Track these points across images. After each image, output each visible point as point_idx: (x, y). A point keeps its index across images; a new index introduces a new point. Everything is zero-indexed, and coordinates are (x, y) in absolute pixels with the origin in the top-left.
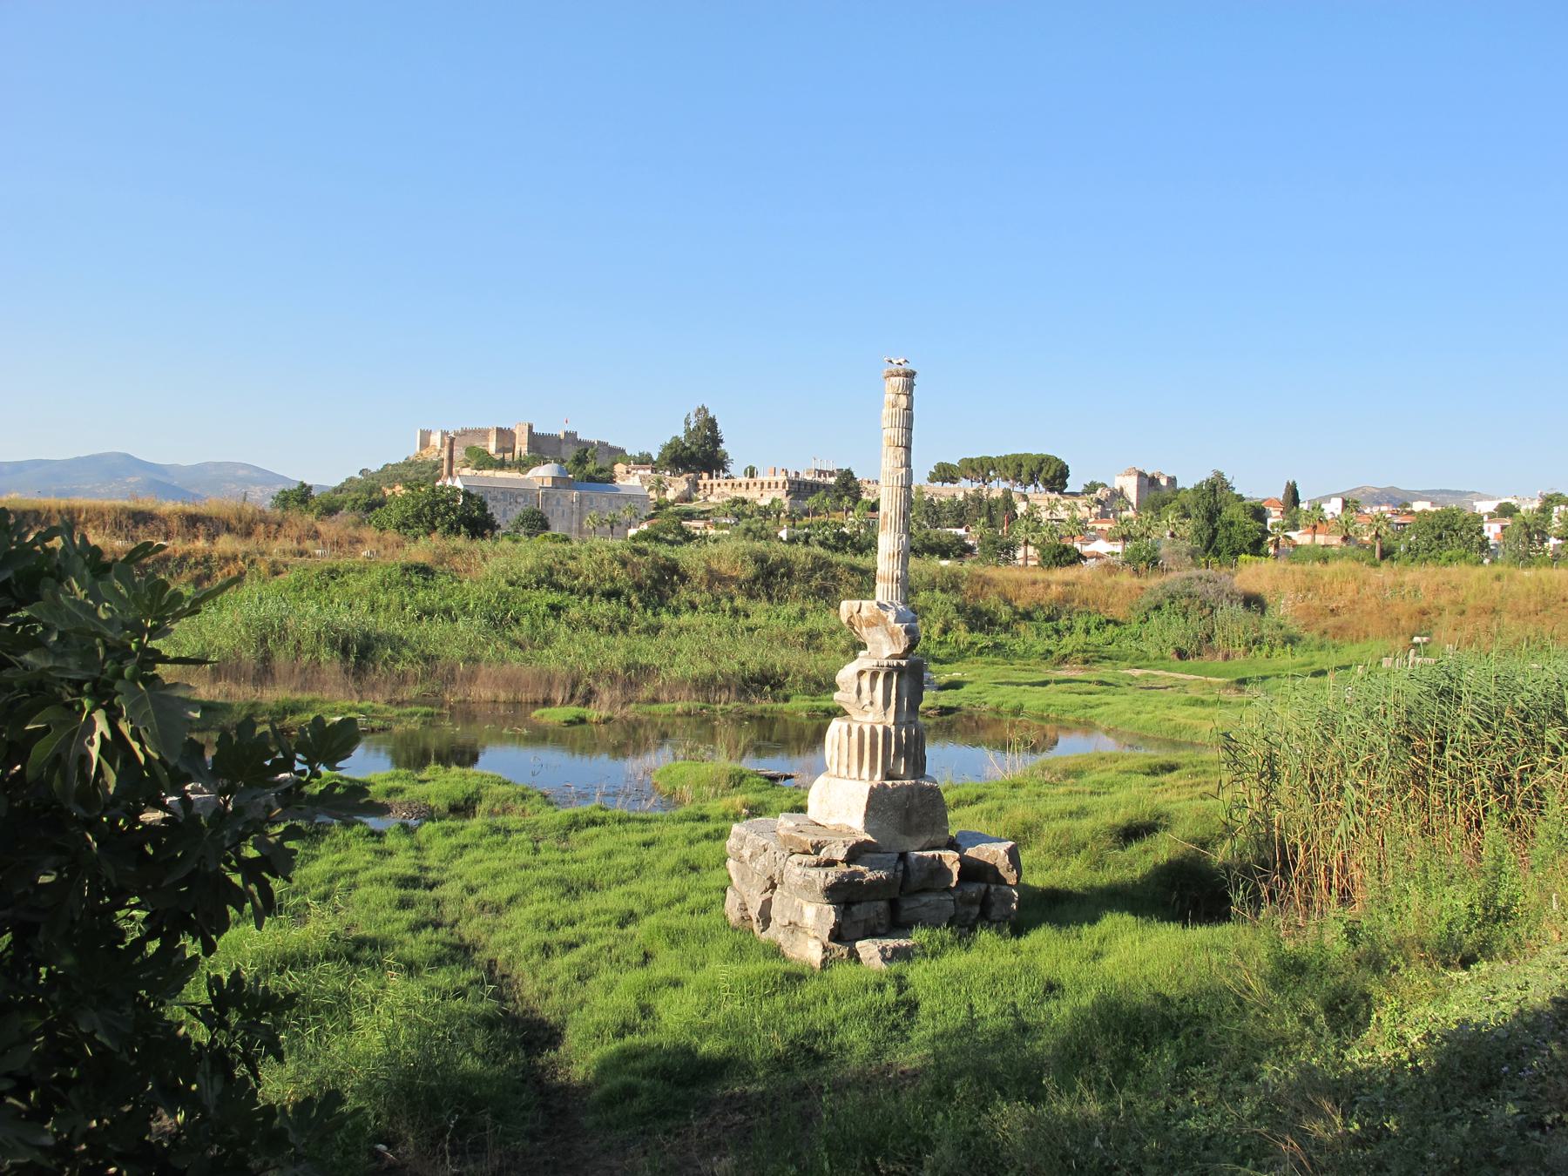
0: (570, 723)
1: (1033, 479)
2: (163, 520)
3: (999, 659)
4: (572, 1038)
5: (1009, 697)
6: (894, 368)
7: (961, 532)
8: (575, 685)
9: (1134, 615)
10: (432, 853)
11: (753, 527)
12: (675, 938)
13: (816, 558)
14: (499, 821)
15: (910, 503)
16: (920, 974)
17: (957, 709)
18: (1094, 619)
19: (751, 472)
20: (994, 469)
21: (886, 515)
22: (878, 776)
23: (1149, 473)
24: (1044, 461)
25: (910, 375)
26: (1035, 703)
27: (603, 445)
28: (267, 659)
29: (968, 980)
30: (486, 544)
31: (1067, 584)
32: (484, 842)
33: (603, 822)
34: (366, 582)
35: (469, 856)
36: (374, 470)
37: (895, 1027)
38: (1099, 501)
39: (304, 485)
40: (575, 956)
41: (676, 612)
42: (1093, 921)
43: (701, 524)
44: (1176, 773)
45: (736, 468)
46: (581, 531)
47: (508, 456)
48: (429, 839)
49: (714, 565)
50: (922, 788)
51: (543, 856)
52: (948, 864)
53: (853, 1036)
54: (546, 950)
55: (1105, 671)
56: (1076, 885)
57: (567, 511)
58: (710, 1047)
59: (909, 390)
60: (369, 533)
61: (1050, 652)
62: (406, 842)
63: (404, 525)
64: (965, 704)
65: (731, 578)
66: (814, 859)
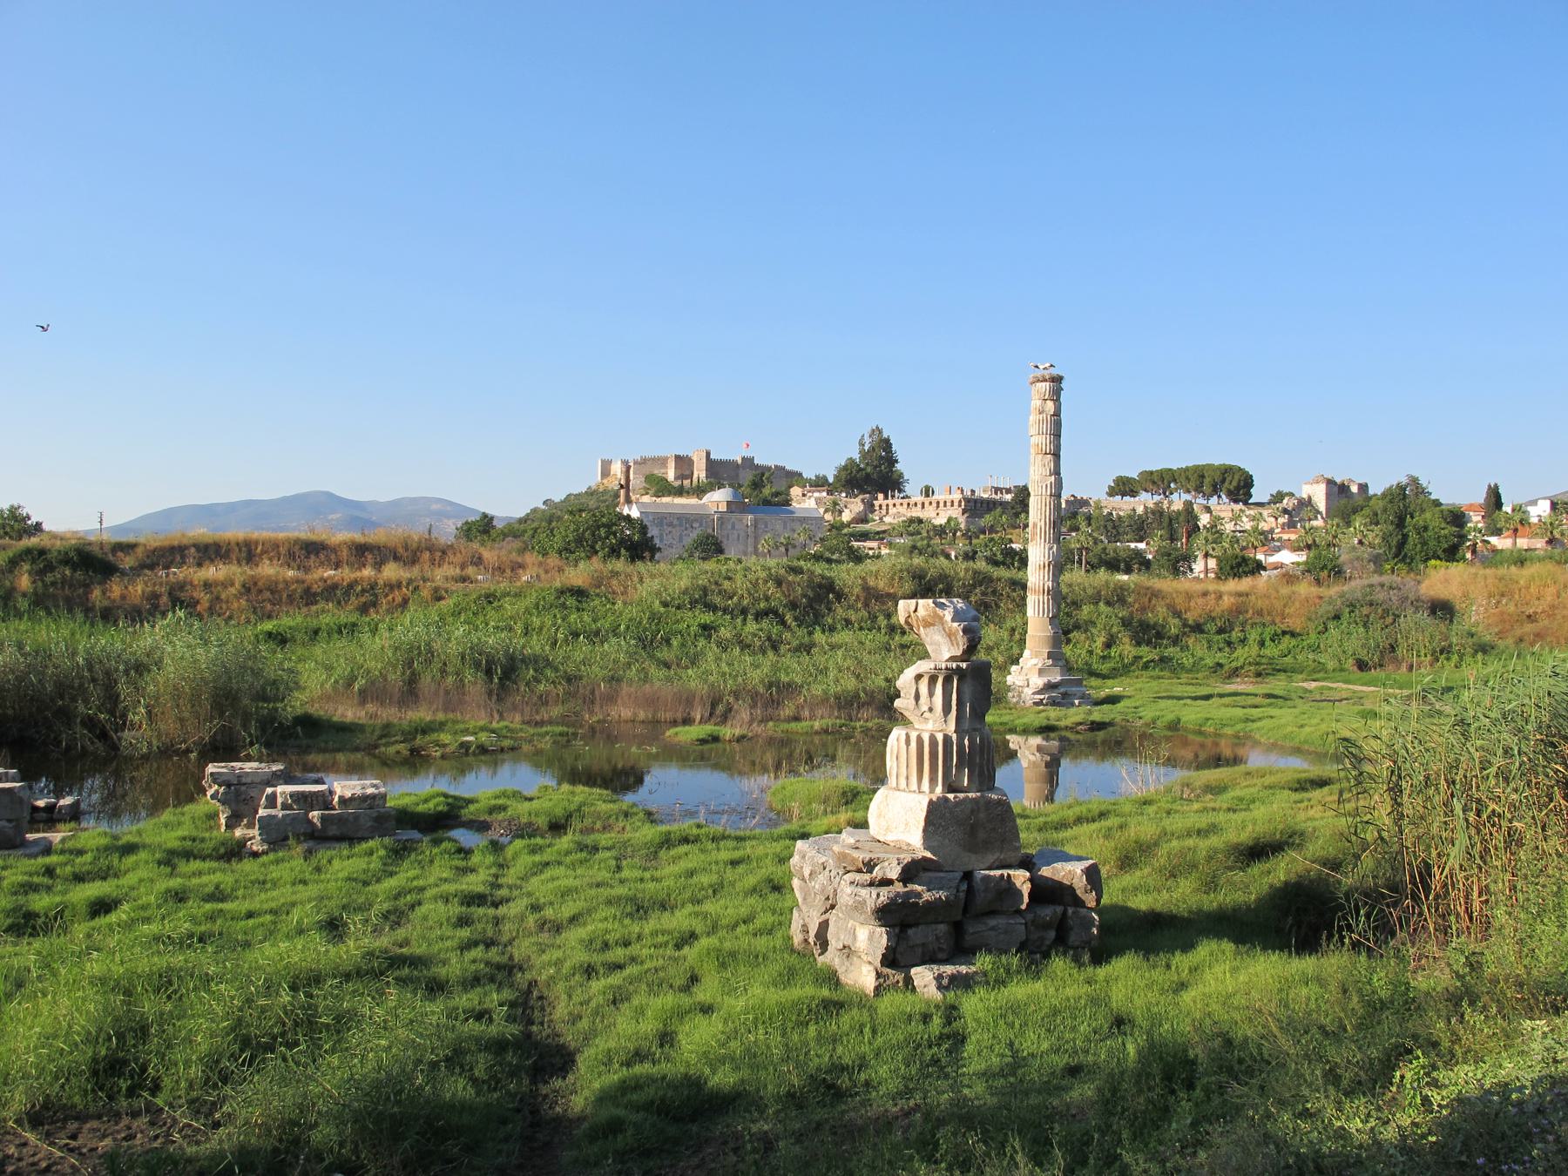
0: (703, 741)
1: (1215, 490)
2: (334, 550)
3: (1166, 673)
4: (583, 1062)
5: (1168, 711)
6: (1039, 373)
7: (1142, 546)
8: (713, 706)
9: (1311, 625)
10: (512, 871)
12: (725, 960)
14: (589, 840)
15: (1068, 516)
16: (973, 1004)
17: (1111, 724)
18: (1269, 631)
19: (928, 491)
20: (1175, 481)
22: (939, 789)
23: (1338, 481)
24: (1227, 471)
25: (1057, 380)
26: (1193, 717)
27: (780, 469)
28: (412, 682)
29: (1026, 1011)
31: (1240, 594)
32: (568, 859)
33: (696, 840)
34: (521, 605)
35: (548, 874)
36: (557, 500)
37: (935, 1061)
38: (1285, 511)
39: (485, 516)
40: (616, 979)
41: (832, 629)
42: (1187, 947)
43: (874, 544)
44: (1326, 789)
45: (913, 489)
46: (756, 552)
47: (687, 482)
48: (516, 855)
49: (871, 583)
50: (990, 801)
51: (626, 874)
52: (1018, 884)
53: (883, 1071)
54: (589, 971)
55: (1277, 685)
56: (1182, 910)
57: (742, 534)
58: (723, 1079)
59: (1056, 395)
60: (530, 558)
61: (1220, 665)
62: (490, 859)
63: (565, 550)
64: (1119, 719)
66: (867, 877)
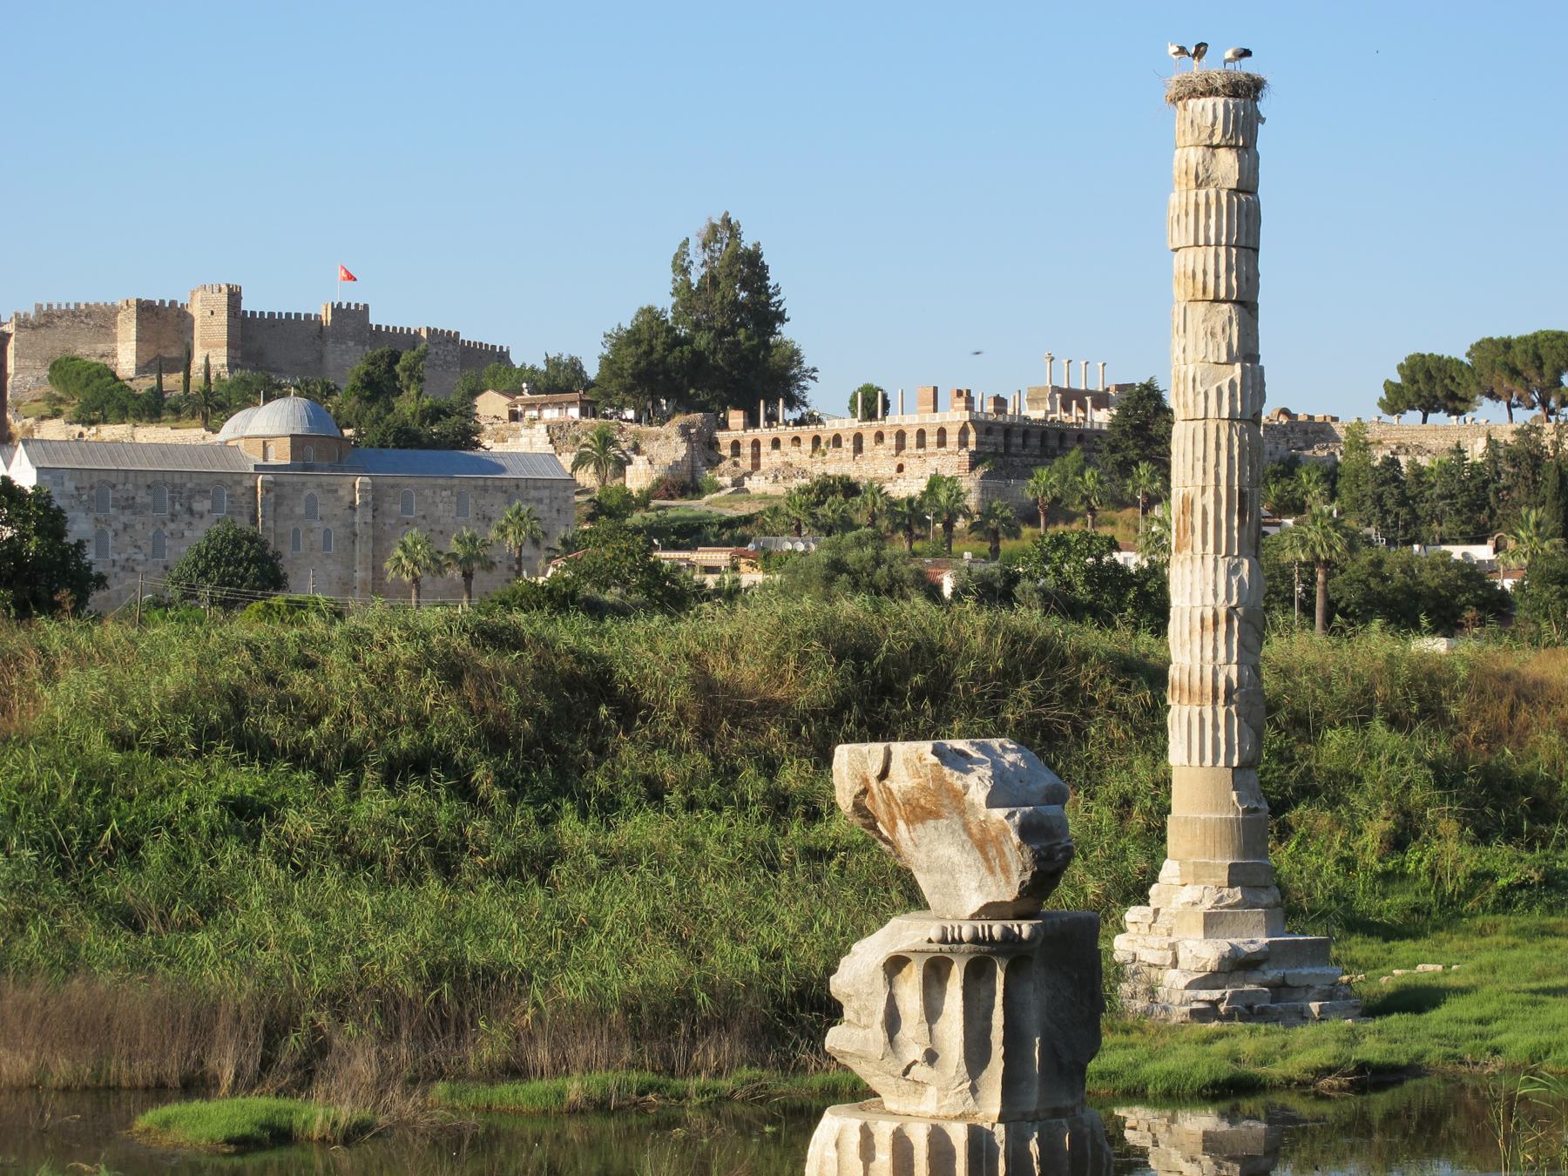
0: (243, 1144)
7: (1483, 553)
8: (274, 1033)
11: (851, 557)
13: (1016, 639)
19: (871, 403)
21: (1188, 505)
25: (1246, 91)
27: (445, 340)
30: (52, 632)
41: (609, 806)
43: (720, 557)
45: (827, 394)
47: (172, 381)
59: (1243, 132)
65: (771, 708)
